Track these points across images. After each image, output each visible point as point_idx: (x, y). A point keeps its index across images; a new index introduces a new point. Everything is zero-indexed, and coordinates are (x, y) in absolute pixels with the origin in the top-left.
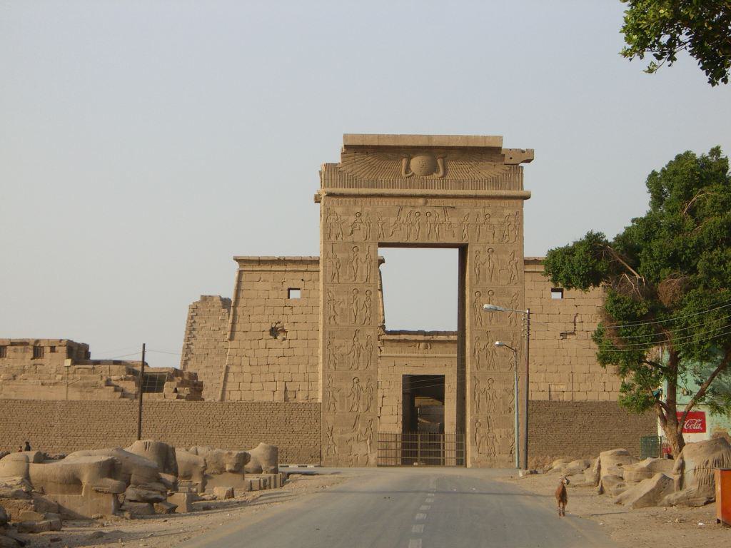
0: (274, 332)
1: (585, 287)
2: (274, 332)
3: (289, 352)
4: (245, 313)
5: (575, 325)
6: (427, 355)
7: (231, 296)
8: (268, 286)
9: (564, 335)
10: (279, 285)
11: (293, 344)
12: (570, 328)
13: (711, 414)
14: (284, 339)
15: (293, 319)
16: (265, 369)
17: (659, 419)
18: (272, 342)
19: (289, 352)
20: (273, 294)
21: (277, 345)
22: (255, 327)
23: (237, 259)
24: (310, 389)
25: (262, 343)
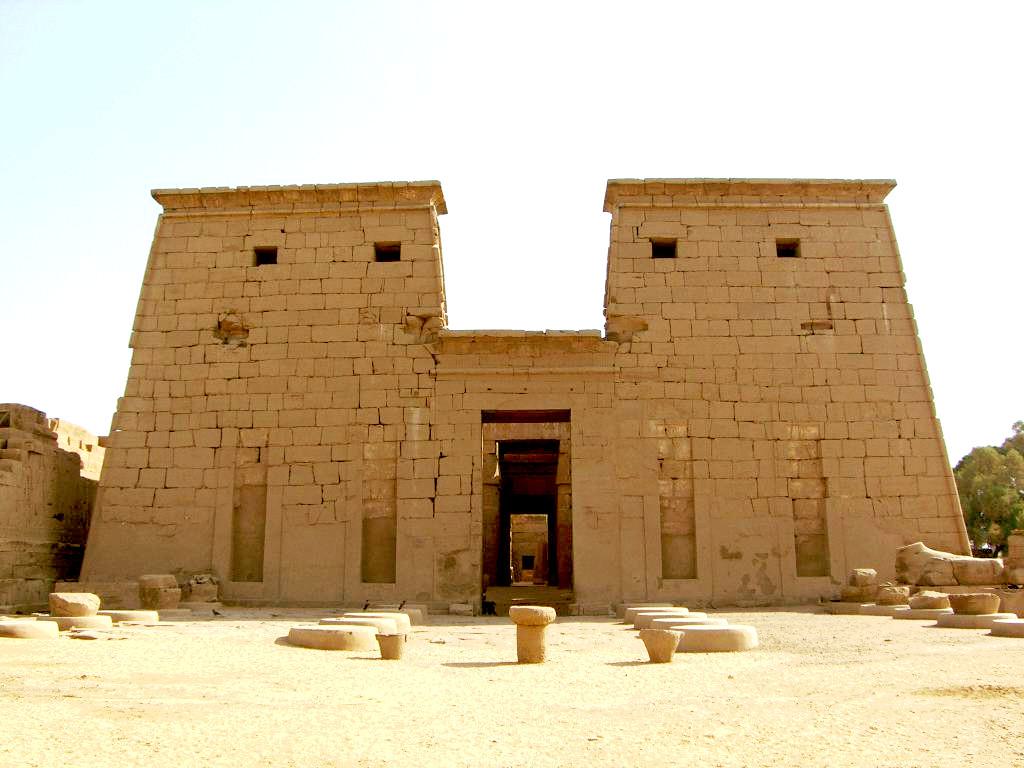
0: (225, 331)
1: (978, 453)
2: (225, 331)
3: (251, 370)
4: (169, 296)
5: (829, 308)
7: (929, 474)
9: (811, 327)
10: (238, 242)
11: (257, 352)
12: (820, 314)
13: (533, 557)
14: (242, 345)
15: (259, 304)
16: (199, 403)
17: (62, 595)
18: (219, 352)
19: (251, 370)
20: (225, 259)
21: (228, 358)
22: (188, 322)
23: (157, 196)
24: (915, 485)
25: (198, 351)
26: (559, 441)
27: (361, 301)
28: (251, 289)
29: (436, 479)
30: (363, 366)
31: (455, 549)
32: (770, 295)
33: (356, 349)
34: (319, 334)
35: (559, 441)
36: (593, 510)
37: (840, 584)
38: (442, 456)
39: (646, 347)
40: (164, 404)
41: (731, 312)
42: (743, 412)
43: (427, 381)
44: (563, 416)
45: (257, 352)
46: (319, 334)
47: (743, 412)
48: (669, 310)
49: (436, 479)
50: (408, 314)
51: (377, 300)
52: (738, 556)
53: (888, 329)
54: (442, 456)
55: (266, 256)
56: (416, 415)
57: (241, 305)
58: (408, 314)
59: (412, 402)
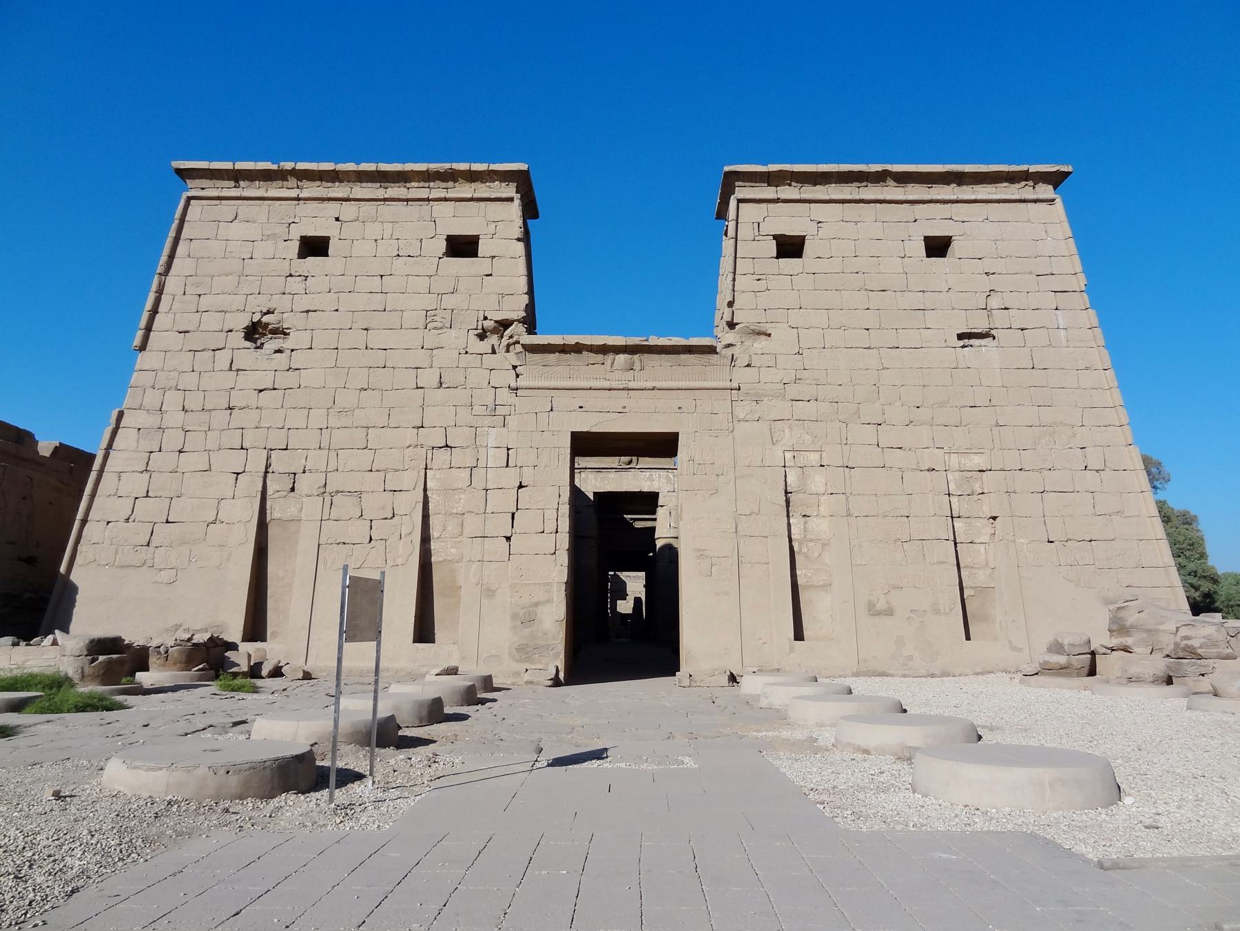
3: (284, 380)
6: (632, 385)
8: (252, 231)
15: (303, 303)
19: (284, 380)
20: (264, 249)
26: (657, 494)
27: (429, 302)
28: (295, 285)
29: (513, 514)
30: (428, 378)
31: (535, 599)
32: (916, 300)
33: (420, 358)
34: (376, 339)
35: (657, 494)
36: (707, 553)
37: (1020, 650)
38: (521, 486)
39: (767, 360)
40: (174, 418)
41: (869, 319)
42: (888, 436)
43: (504, 396)
44: (662, 446)
45: (298, 359)
46: (376, 339)
47: (888, 436)
48: (796, 318)
49: (513, 514)
50: (485, 318)
51: (449, 301)
52: (889, 612)
53: (1064, 340)
54: (521, 486)
55: (314, 247)
56: (493, 437)
57: (277, 302)
58: (485, 318)
59: (488, 421)
